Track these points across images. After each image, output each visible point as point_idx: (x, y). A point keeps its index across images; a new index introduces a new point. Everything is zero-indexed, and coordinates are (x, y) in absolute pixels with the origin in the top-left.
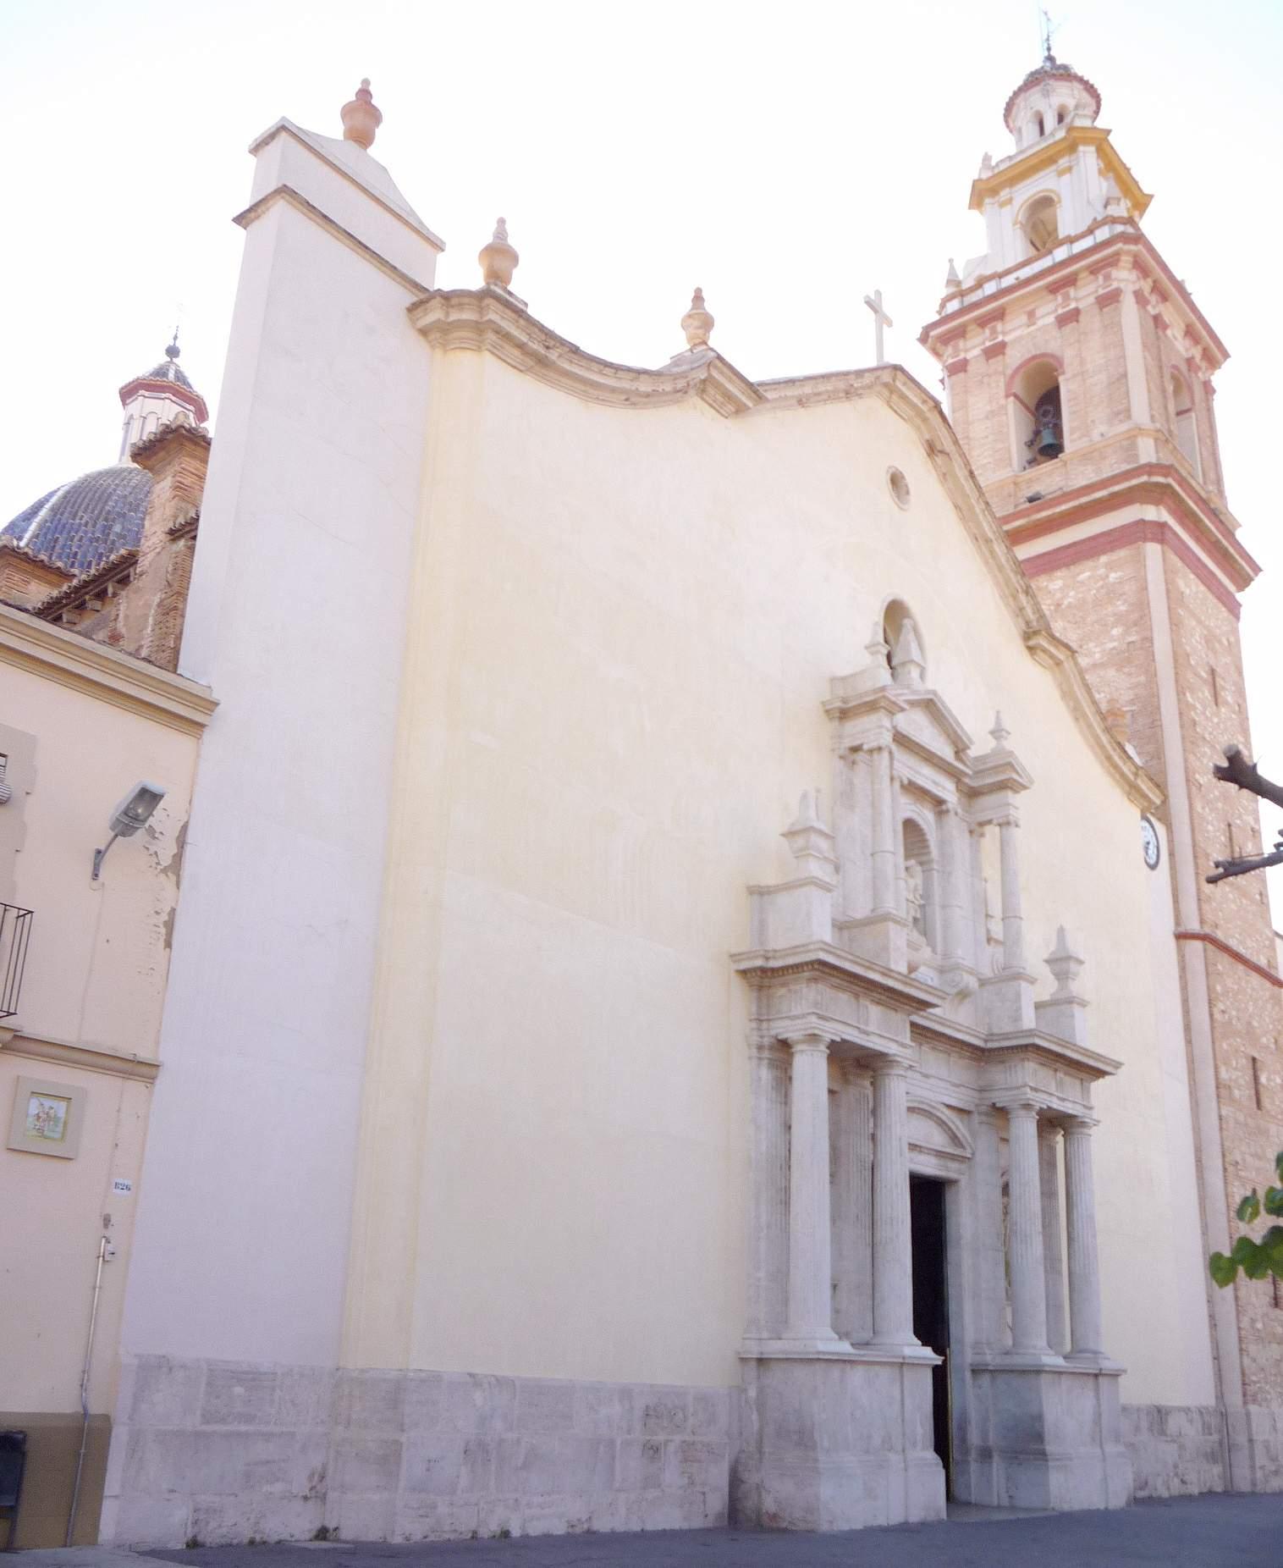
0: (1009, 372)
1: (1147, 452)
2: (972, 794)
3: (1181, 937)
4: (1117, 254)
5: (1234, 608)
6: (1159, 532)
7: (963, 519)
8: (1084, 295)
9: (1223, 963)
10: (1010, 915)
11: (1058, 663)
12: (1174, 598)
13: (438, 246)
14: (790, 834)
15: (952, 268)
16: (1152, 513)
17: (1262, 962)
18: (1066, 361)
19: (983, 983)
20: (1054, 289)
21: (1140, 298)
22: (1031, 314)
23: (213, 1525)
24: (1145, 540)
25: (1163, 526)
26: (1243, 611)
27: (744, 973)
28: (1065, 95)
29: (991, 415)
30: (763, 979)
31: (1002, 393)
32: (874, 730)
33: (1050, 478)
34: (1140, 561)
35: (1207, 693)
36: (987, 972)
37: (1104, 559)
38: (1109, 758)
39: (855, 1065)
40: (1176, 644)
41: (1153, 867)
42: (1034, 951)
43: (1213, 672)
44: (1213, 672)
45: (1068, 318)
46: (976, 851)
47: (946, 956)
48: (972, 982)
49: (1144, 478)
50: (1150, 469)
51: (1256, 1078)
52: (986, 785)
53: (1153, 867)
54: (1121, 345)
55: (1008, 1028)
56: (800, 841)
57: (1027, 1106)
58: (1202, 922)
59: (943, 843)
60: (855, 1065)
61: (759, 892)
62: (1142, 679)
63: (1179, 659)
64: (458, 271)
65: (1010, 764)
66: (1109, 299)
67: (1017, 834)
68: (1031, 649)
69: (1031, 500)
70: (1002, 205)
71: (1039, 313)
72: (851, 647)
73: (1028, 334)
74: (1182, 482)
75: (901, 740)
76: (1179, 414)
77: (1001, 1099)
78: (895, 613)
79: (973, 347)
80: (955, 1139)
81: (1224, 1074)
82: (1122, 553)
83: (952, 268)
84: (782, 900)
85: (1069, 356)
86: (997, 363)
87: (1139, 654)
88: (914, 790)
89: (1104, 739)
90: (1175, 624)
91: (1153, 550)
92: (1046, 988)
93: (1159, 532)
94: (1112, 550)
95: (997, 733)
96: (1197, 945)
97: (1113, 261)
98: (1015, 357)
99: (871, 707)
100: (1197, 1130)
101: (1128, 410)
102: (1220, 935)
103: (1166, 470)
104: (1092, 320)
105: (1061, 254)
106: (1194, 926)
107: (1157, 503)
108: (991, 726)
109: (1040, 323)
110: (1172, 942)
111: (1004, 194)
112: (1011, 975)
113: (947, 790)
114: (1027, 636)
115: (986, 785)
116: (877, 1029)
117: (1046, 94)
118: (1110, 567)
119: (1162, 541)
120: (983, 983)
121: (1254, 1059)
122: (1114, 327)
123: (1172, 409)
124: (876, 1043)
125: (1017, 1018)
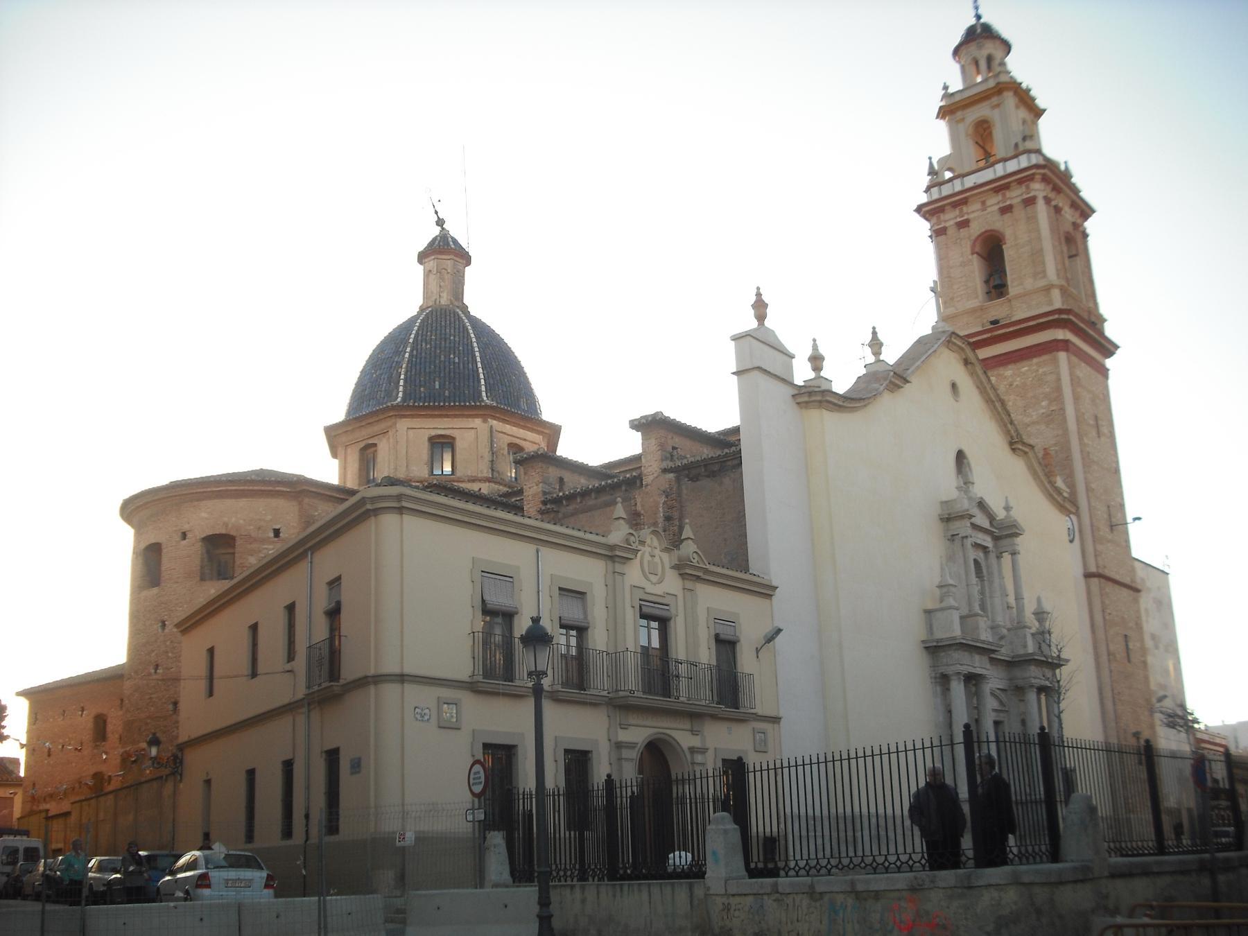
0: (973, 238)
1: (1058, 304)
2: (996, 539)
3: (1088, 576)
4: (1033, 174)
5: (1104, 372)
6: (1065, 345)
7: (981, 392)
8: (1015, 195)
9: (1109, 588)
10: (1019, 598)
11: (1026, 453)
12: (1075, 381)
13: (792, 357)
14: (940, 587)
15: (931, 164)
16: (1061, 334)
17: (1127, 580)
18: (1007, 237)
19: (1009, 630)
20: (997, 190)
21: (1047, 200)
22: (983, 203)
23: (1150, 844)
24: (1058, 350)
25: (1066, 342)
26: (1110, 373)
27: (926, 648)
28: (990, 48)
29: (963, 264)
30: (934, 649)
31: (969, 251)
32: (963, 528)
33: (998, 310)
34: (1055, 362)
35: (1094, 433)
36: (1009, 626)
37: (1035, 360)
38: (1051, 495)
39: (972, 680)
40: (1077, 410)
41: (1071, 541)
42: (1029, 607)
43: (1096, 418)
44: (1096, 418)
45: (1006, 210)
46: (999, 565)
47: (993, 621)
48: (1005, 631)
49: (1056, 316)
50: (1060, 311)
51: (1127, 646)
52: (1003, 534)
53: (1071, 541)
54: (1038, 231)
55: (1022, 652)
56: (945, 590)
57: (1032, 686)
58: (1098, 567)
59: (988, 567)
60: (972, 680)
61: (928, 612)
62: (1060, 432)
63: (1079, 420)
64: (802, 373)
65: (1015, 526)
66: (1030, 202)
67: (1019, 557)
68: (1014, 450)
69: (993, 323)
70: (958, 122)
71: (989, 203)
72: (947, 485)
73: (983, 218)
74: (1076, 315)
75: (974, 526)
76: (1070, 257)
77: (1020, 683)
78: (960, 456)
79: (950, 218)
80: (1001, 703)
81: (1112, 648)
82: (1045, 357)
83: (931, 164)
84: (939, 614)
85: (1008, 234)
86: (964, 232)
87: (1056, 417)
88: (977, 546)
89: (1048, 486)
90: (1077, 399)
91: (1062, 356)
92: (1035, 625)
93: (1065, 345)
94: (1040, 355)
95: (1007, 508)
96: (1096, 580)
97: (1031, 178)
98: (976, 229)
99: (962, 517)
100: (1099, 678)
101: (1044, 272)
102: (1107, 573)
103: (1068, 311)
104: (1019, 213)
105: (1000, 170)
106: (1093, 569)
107: (1063, 327)
108: (1003, 505)
109: (989, 210)
110: (1082, 580)
111: (959, 114)
112: (1020, 626)
113: (988, 541)
114: (1011, 444)
115: (1003, 534)
116: (978, 664)
117: (980, 47)
118: (1038, 365)
119: (1067, 350)
120: (1009, 630)
121: (1126, 636)
122: (1032, 219)
123: (1066, 255)
124: (979, 671)
125: (1025, 646)
